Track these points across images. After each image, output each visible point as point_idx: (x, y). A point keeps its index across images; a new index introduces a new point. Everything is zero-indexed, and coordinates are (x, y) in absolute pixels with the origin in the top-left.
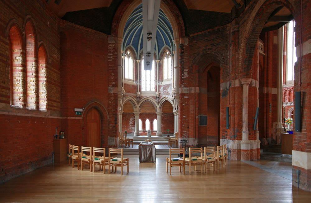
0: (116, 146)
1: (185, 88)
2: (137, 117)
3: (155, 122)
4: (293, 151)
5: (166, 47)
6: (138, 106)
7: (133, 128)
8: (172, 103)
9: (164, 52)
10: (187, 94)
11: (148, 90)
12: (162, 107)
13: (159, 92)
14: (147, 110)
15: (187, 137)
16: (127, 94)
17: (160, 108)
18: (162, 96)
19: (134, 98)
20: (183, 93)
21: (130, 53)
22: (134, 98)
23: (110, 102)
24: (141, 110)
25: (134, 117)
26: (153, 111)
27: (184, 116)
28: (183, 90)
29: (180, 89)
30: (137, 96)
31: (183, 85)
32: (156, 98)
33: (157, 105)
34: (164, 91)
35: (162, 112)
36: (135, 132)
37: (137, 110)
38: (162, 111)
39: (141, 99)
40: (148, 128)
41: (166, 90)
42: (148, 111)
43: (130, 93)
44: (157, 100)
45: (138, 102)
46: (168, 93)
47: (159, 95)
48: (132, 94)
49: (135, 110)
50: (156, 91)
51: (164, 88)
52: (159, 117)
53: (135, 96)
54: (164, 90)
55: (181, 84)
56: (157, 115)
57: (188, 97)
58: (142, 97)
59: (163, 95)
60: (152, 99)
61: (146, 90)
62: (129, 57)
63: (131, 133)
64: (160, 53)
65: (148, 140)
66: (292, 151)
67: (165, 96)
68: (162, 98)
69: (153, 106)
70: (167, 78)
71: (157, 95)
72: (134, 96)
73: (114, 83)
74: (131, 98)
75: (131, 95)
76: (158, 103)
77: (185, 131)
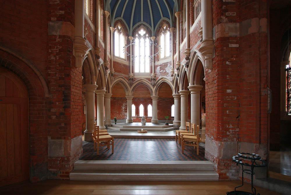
0: (66, 159)
1: (232, 25)
2: (129, 101)
3: (150, 107)
5: (163, 20)
6: (130, 89)
7: (126, 113)
8: (171, 84)
9: (161, 27)
10: (236, 37)
11: (142, 71)
13: (155, 73)
14: (141, 94)
15: (235, 139)
16: (117, 74)
17: (156, 90)
18: (158, 78)
19: (126, 79)
20: (227, 36)
21: (121, 28)
22: (126, 79)
23: (53, 58)
24: (134, 94)
25: (127, 102)
26: (147, 96)
27: (229, 91)
28: (227, 29)
29: (217, 28)
30: (129, 77)
31: (227, 17)
32: (152, 80)
33: (152, 87)
34: (161, 71)
35: (158, 97)
36: (128, 118)
37: (129, 94)
39: (135, 81)
40: (142, 114)
42: (141, 96)
43: (122, 73)
44: (153, 82)
45: (131, 85)
46: (166, 73)
47: (155, 77)
49: (127, 94)
50: (151, 72)
51: (160, 68)
52: (154, 102)
53: (127, 78)
54: (161, 70)
55: (222, 14)
56: (152, 99)
57: (237, 46)
58: (135, 78)
59: (160, 76)
60: (147, 81)
61: (140, 71)
62: (119, 32)
63: (124, 119)
64: (155, 29)
65: (142, 129)
68: (158, 79)
69: (148, 90)
70: (165, 57)
71: (153, 77)
72: (125, 77)
73: (62, 12)
74: (122, 79)
75: (122, 76)
76: (154, 86)
77: (231, 126)
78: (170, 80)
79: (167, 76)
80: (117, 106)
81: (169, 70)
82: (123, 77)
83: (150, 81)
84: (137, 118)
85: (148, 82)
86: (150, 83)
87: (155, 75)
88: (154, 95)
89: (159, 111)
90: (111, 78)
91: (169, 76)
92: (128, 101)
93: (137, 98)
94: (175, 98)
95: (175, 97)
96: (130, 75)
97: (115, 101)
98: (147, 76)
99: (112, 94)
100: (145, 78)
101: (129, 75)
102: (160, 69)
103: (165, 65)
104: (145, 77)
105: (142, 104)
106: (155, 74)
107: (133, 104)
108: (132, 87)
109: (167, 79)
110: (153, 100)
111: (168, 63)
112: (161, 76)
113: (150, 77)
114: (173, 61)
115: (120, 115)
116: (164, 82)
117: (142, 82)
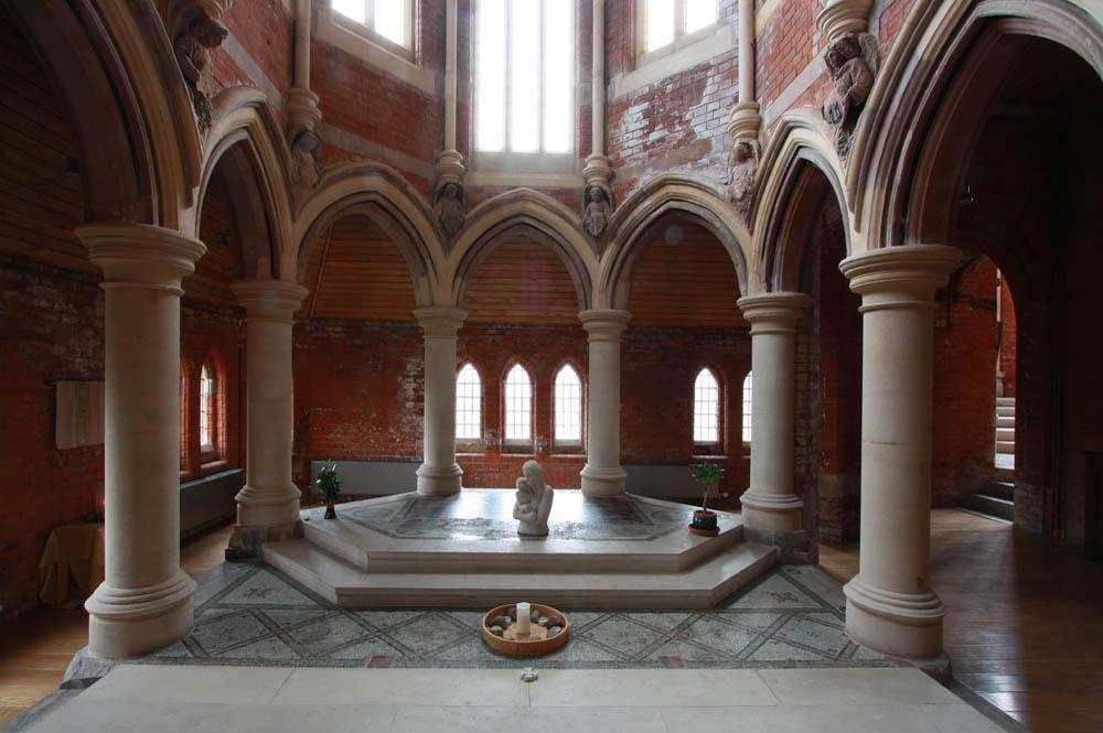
2: (440, 345)
3: (567, 381)
4: (1013, 468)
6: (447, 263)
11: (524, 145)
12: (626, 272)
14: (524, 304)
16: (341, 138)
17: (614, 276)
18: (631, 184)
22: (412, 189)
32: (588, 200)
33: (585, 249)
34: (654, 136)
36: (428, 460)
37: (438, 292)
38: (628, 306)
39: (474, 205)
40: (518, 426)
41: (669, 122)
42: (517, 314)
45: (449, 232)
47: (610, 178)
48: (390, 153)
49: (422, 295)
50: (585, 148)
51: (647, 114)
52: (601, 352)
54: (650, 128)
56: (586, 334)
58: (479, 190)
59: (642, 170)
66: (1016, 465)
67: (662, 174)
70: (679, 34)
78: (720, 190)
79: (702, 168)
81: (714, 120)
82: (389, 168)
84: (489, 449)
85: (563, 216)
86: (577, 221)
87: (610, 164)
88: (599, 303)
89: (827, 542)
90: (291, 162)
91: (712, 162)
92: (431, 344)
93: (491, 324)
94: (755, 328)
95: (872, 289)
96: (447, 161)
97: (358, 342)
99: (304, 292)
101: (437, 161)
102: (646, 122)
103: (688, 87)
105: (523, 364)
106: (611, 157)
107: (467, 361)
109: (699, 187)
111: (707, 67)
112: (650, 170)
113: (575, 183)
114: (754, 47)
116: (670, 210)
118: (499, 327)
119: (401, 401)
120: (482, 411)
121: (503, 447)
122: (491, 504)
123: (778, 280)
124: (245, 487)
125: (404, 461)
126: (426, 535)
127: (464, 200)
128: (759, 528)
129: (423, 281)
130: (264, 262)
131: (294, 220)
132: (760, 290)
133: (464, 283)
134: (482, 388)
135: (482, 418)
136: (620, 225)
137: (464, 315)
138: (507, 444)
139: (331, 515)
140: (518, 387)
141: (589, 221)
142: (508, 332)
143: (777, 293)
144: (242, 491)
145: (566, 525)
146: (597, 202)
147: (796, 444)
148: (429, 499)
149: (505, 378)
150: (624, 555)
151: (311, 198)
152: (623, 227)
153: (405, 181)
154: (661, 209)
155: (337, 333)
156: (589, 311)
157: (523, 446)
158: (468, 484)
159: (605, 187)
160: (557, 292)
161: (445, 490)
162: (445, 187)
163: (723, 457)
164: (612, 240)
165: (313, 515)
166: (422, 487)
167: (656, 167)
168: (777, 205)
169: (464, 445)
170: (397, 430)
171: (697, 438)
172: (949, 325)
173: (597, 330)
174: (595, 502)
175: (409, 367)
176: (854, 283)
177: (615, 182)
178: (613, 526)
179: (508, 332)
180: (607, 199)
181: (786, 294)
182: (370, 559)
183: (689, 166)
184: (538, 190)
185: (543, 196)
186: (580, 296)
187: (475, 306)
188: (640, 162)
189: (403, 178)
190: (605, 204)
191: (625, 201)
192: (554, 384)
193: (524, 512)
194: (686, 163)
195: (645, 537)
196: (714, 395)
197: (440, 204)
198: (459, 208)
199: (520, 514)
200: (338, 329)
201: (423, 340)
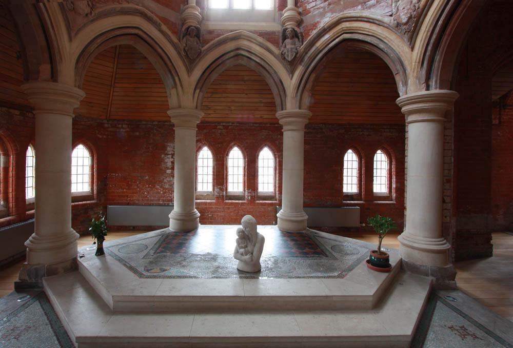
2: (185, 135)
3: (266, 157)
14: (238, 109)
17: (301, 87)
18: (315, 25)
22: (164, 28)
26: (262, 115)
30: (183, 24)
32: (285, 38)
33: (281, 71)
36: (176, 209)
37: (183, 97)
39: (207, 42)
40: (236, 184)
42: (239, 116)
44: (289, 47)
45: (191, 59)
47: (300, 23)
49: (173, 101)
52: (292, 139)
56: (281, 127)
58: (210, 32)
59: (322, 15)
76: (292, 65)
78: (387, 20)
79: (370, 7)
80: (135, 152)
83: (275, 42)
84: (218, 198)
87: (300, 14)
92: (178, 132)
93: (219, 123)
97: (137, 134)
98: (264, 24)
100: (255, 32)
104: (253, 29)
105: (238, 146)
107: (204, 145)
108: (197, 73)
110: (285, 128)
112: (329, 15)
113: (276, 28)
115: (154, 186)
117: (238, 49)
118: (224, 124)
119: (164, 169)
120: (214, 175)
121: (226, 196)
122: (219, 236)
123: (436, 82)
124: (33, 235)
125: (165, 205)
126: (167, 273)
127: (201, 38)
128: (419, 263)
129: (174, 91)
130: (45, 69)
131: (70, 39)
132: (420, 90)
133: (201, 94)
134: (214, 161)
135: (214, 179)
136: (306, 53)
137: (201, 114)
138: (228, 194)
139: (100, 252)
140: (236, 161)
141: (285, 51)
142: (230, 127)
143: (434, 91)
144: (30, 238)
145: (272, 260)
146: (291, 39)
147: (444, 201)
148: (176, 235)
149: (227, 155)
150: (327, 297)
151: (85, 25)
152: (309, 54)
153: (159, 21)
154: (337, 40)
155: (124, 128)
156: (284, 111)
157: (239, 196)
158: (205, 221)
159: (296, 29)
160: (261, 102)
161: (188, 229)
162: (189, 27)
163: (362, 202)
164: (300, 64)
165: (86, 247)
166: (172, 226)
167: (332, 11)
168: (440, 22)
169: (203, 196)
170: (161, 187)
171: (345, 190)
172: (500, 122)
173: (289, 123)
174: (288, 237)
175: (169, 149)
176: (404, 109)
177: (303, 25)
178: (309, 261)
179: (230, 127)
180: (298, 37)
181: (438, 91)
182: (114, 301)
183: (360, 7)
184: (251, 32)
185: (255, 36)
186: (278, 101)
187: (209, 112)
188: (321, 10)
189: (158, 19)
190: (296, 40)
191: (310, 37)
192: (258, 158)
193: (242, 254)
194: (357, 6)
195: (336, 274)
196: (356, 165)
197: (185, 39)
198: (197, 44)
199: (239, 256)
200: (124, 126)
201: (174, 130)
